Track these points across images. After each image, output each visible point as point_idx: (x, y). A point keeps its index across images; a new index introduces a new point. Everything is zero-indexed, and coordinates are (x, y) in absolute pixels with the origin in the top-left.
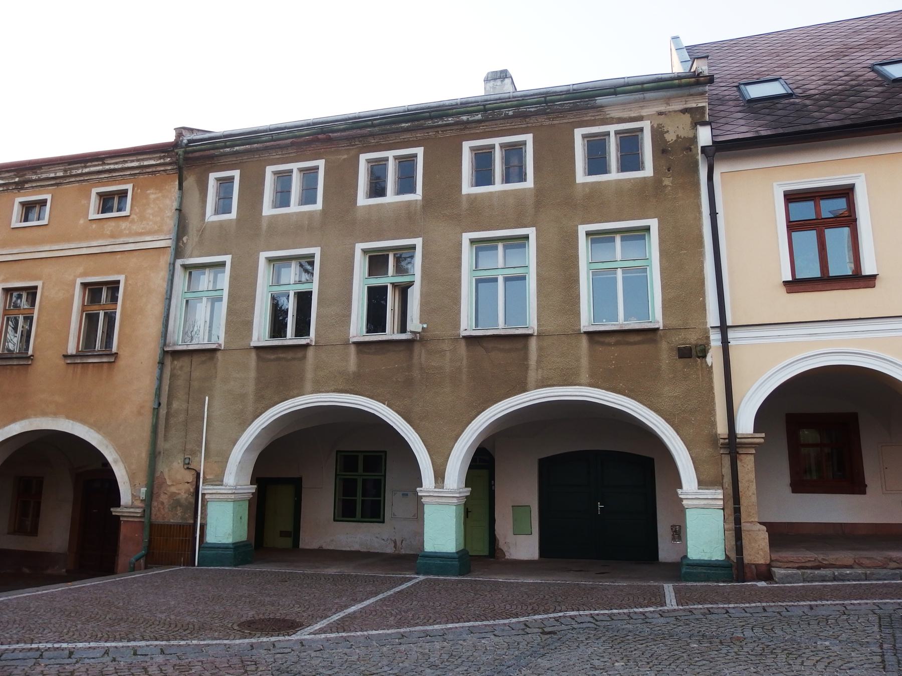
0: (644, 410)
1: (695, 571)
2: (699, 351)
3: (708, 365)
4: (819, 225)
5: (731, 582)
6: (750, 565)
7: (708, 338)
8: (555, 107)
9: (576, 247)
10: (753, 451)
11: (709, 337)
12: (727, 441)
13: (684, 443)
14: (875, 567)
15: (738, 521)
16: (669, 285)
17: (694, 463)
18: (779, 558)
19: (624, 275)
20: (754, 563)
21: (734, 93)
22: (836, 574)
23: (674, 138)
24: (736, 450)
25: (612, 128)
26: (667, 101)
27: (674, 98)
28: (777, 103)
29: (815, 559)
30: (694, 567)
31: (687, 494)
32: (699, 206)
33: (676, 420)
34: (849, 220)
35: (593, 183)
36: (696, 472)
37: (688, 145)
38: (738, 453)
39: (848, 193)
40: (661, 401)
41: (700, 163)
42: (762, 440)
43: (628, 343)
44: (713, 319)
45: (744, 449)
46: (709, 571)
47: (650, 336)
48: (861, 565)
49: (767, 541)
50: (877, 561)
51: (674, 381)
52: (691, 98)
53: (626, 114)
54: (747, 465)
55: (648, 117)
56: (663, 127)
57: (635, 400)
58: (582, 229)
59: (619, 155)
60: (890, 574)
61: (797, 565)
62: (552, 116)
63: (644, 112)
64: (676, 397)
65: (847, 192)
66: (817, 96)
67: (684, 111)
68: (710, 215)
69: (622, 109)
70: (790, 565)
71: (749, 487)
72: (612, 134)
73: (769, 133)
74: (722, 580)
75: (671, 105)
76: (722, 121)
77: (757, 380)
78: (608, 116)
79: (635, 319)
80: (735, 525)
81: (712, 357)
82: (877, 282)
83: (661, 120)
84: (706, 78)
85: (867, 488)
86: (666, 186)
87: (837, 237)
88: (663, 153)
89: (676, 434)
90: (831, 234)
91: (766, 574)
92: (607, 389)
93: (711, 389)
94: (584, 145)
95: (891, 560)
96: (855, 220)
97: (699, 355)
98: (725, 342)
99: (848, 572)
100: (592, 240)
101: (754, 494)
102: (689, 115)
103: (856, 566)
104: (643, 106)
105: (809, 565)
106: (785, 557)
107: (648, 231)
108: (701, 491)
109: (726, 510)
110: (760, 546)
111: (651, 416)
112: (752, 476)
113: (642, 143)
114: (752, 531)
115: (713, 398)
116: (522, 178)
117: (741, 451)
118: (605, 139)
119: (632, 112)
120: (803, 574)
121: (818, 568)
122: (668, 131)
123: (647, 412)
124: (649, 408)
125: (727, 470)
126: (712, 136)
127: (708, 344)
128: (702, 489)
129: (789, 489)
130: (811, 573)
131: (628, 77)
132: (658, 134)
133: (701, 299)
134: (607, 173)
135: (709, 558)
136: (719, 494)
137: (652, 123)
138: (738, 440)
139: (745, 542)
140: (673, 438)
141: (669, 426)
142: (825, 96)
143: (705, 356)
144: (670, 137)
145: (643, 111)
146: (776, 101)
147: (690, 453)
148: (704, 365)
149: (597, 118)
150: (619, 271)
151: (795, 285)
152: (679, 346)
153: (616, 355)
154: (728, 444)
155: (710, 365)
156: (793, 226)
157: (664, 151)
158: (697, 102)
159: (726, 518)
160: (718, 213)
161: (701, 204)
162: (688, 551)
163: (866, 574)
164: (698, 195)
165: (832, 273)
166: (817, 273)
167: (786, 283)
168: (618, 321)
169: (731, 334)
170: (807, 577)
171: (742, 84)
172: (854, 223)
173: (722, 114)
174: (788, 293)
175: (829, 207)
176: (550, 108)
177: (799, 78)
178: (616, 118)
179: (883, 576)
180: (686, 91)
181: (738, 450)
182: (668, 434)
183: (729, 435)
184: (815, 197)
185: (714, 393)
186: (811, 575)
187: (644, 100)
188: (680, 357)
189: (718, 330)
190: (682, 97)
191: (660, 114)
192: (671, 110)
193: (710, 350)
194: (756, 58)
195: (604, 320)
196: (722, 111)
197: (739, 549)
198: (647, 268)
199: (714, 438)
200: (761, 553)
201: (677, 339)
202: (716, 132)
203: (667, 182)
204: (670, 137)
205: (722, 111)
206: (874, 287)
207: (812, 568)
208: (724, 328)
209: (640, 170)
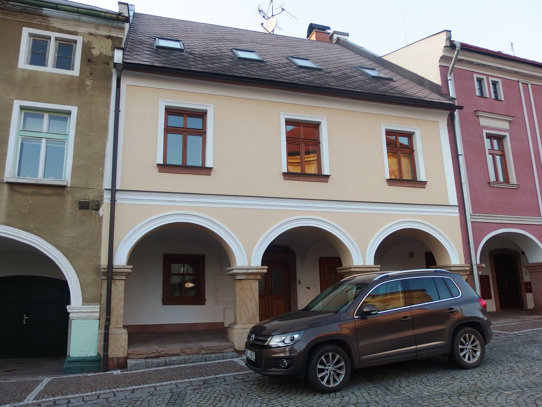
0: (47, 246)
1: (73, 366)
2: (94, 205)
3: (100, 216)
4: (185, 132)
5: (99, 372)
6: (113, 359)
7: (102, 196)
8: (8, 5)
9: (9, 116)
10: (124, 278)
11: (103, 196)
12: (106, 270)
13: (76, 271)
14: (193, 354)
15: (107, 328)
16: (79, 155)
17: (81, 286)
18: (133, 352)
19: (39, 144)
20: (116, 357)
21: (151, 41)
22: (167, 361)
23: (98, 54)
24: (112, 277)
25: (53, 35)
26: (97, 26)
27: (101, 26)
28: (173, 53)
29: (157, 351)
30: (73, 363)
31: (73, 309)
32: (108, 104)
33: (72, 254)
34: (202, 133)
35: (31, 71)
36: (82, 293)
37: (107, 60)
38: (113, 279)
39: (203, 116)
40: (61, 239)
41: (114, 74)
42: (130, 270)
43: (41, 195)
44: (107, 184)
45: (117, 276)
46: (84, 365)
47: (59, 191)
48: (184, 353)
49: (127, 340)
50: (194, 350)
51: (74, 225)
52: (113, 30)
53: (65, 28)
54: (119, 288)
55: (82, 34)
56: (92, 44)
57: (41, 237)
58: (17, 104)
59: (56, 56)
60: (199, 358)
61: (145, 356)
62: (5, 12)
63: (79, 30)
64: (73, 237)
65: (202, 115)
66: (197, 55)
67: (108, 37)
68: (115, 111)
69: (63, 23)
70: (140, 356)
71: (119, 303)
72: (53, 39)
73: (160, 65)
74: (93, 371)
75: (99, 30)
76: (136, 53)
77: (132, 229)
78: (51, 25)
79: (54, 178)
80: (105, 331)
81: (103, 210)
82: (213, 173)
83: (91, 39)
84: (124, 17)
85: (206, 302)
86: (87, 85)
87: (194, 141)
88: (88, 62)
89: (70, 265)
90: (191, 139)
91: (122, 364)
92: (20, 228)
93: (100, 232)
94: (30, 42)
95: (202, 348)
96: (205, 133)
97: (94, 208)
98: (113, 201)
99: (175, 359)
100: (25, 114)
101: (122, 308)
102: (111, 41)
103: (181, 354)
104: (80, 25)
105: (153, 355)
106: (138, 351)
107: (478, 266)
108: (84, 306)
109: (101, 320)
110: (122, 344)
111: (52, 251)
112: (122, 295)
113: (75, 52)
114: (117, 334)
115: (101, 239)
116: (69, 66)
117: (115, 278)
118: (47, 42)
119: (70, 27)
120: (146, 363)
121: (158, 357)
122: (94, 48)
123: (50, 248)
124: (52, 244)
125: (104, 292)
126: (123, 58)
127: (102, 200)
128: (85, 305)
129: (161, 302)
130: (151, 362)
131: (70, 2)
132: (87, 48)
133: (101, 169)
134: (44, 66)
135: (85, 355)
136: (96, 308)
137: (84, 39)
138: (114, 270)
139: (111, 342)
140: (68, 267)
141: (66, 258)
142: (202, 56)
143: (98, 209)
144: (96, 52)
145: (79, 28)
146: (174, 51)
147: (79, 279)
148: (97, 216)
149: (43, 24)
150: (44, 141)
151: (164, 167)
152: (80, 200)
153: (30, 202)
154: (107, 272)
155: (101, 216)
156: (168, 130)
157: (89, 61)
158: (117, 33)
159: (100, 326)
160: (120, 111)
161: (110, 103)
162: (71, 351)
163: (185, 359)
164: (109, 97)
165: (189, 163)
166: (180, 163)
167: (159, 165)
168: (37, 178)
169: (118, 196)
170: (148, 365)
171: (157, 37)
172: (204, 134)
173: (138, 49)
174: (159, 172)
175: (194, 123)
176: (3, 5)
177: (192, 44)
178: (57, 28)
179: (195, 360)
180: (110, 23)
181: (113, 277)
182: (64, 264)
183: (108, 266)
184: (184, 113)
185: (101, 236)
186: (151, 363)
187: (79, 20)
188: (81, 208)
189: (110, 192)
190: (107, 26)
191: (91, 34)
192: (99, 34)
193: (103, 205)
194: (174, 29)
195: (29, 176)
196: (139, 48)
197: (106, 348)
198: (65, 142)
199: (98, 268)
200: (122, 349)
201: (80, 195)
202: (126, 57)
203: (88, 82)
204: (96, 52)
205: (139, 48)
206: (210, 175)
207: (154, 357)
208: (113, 191)
209: (70, 70)
